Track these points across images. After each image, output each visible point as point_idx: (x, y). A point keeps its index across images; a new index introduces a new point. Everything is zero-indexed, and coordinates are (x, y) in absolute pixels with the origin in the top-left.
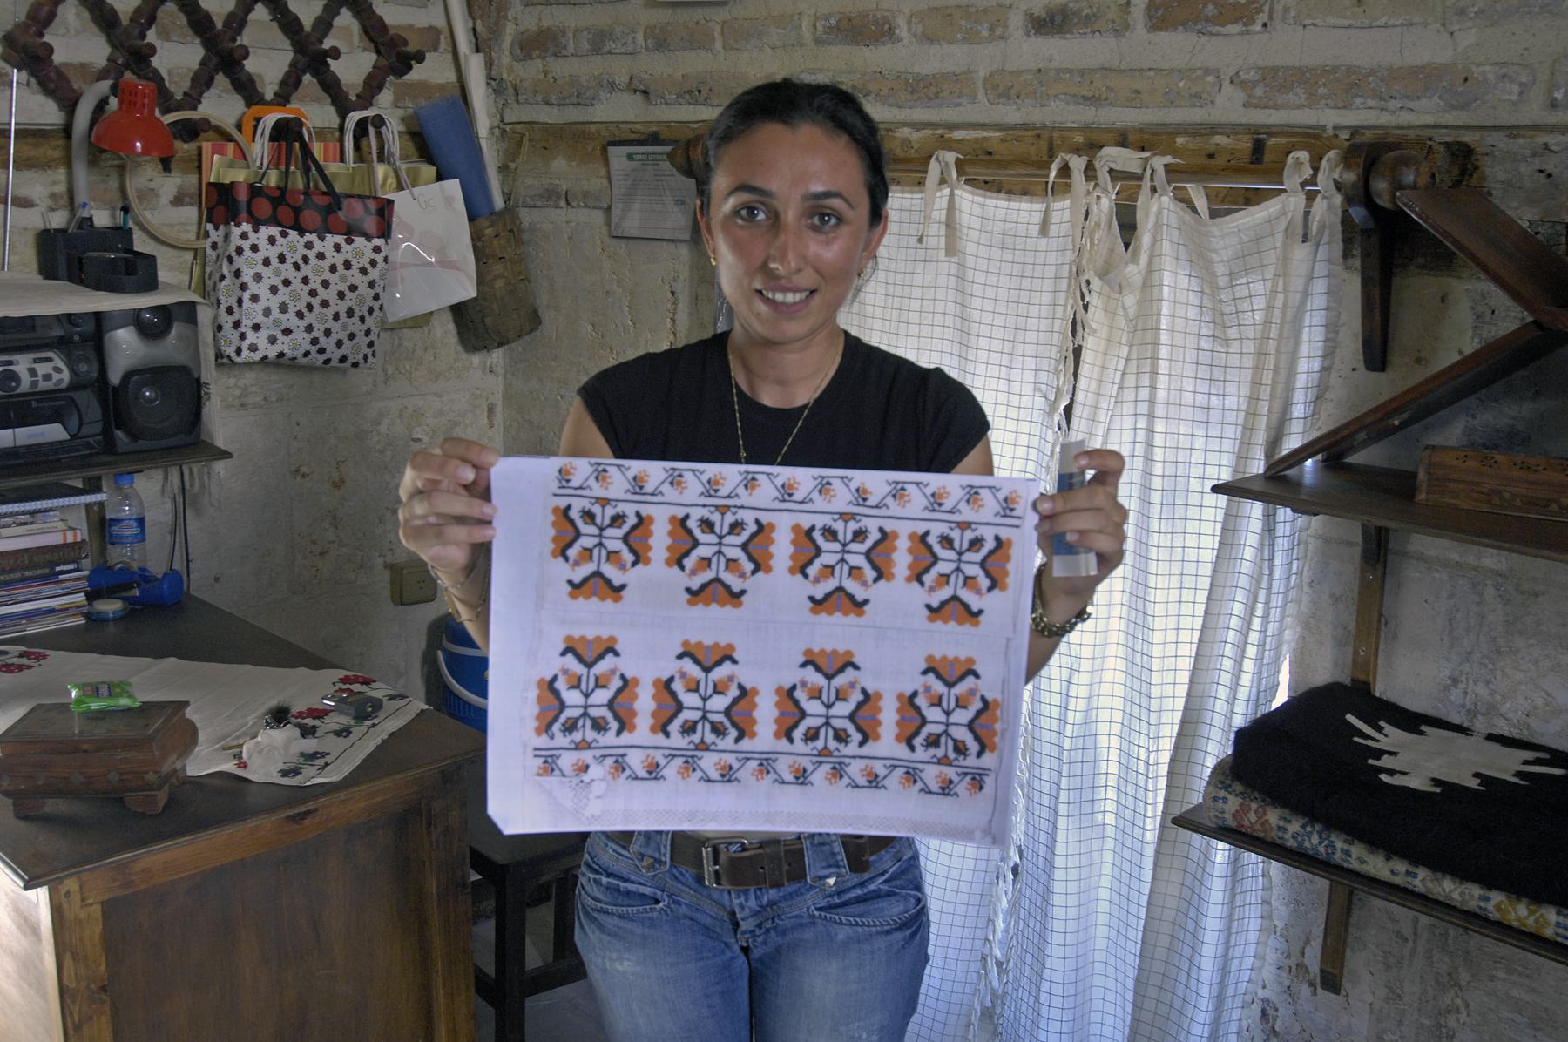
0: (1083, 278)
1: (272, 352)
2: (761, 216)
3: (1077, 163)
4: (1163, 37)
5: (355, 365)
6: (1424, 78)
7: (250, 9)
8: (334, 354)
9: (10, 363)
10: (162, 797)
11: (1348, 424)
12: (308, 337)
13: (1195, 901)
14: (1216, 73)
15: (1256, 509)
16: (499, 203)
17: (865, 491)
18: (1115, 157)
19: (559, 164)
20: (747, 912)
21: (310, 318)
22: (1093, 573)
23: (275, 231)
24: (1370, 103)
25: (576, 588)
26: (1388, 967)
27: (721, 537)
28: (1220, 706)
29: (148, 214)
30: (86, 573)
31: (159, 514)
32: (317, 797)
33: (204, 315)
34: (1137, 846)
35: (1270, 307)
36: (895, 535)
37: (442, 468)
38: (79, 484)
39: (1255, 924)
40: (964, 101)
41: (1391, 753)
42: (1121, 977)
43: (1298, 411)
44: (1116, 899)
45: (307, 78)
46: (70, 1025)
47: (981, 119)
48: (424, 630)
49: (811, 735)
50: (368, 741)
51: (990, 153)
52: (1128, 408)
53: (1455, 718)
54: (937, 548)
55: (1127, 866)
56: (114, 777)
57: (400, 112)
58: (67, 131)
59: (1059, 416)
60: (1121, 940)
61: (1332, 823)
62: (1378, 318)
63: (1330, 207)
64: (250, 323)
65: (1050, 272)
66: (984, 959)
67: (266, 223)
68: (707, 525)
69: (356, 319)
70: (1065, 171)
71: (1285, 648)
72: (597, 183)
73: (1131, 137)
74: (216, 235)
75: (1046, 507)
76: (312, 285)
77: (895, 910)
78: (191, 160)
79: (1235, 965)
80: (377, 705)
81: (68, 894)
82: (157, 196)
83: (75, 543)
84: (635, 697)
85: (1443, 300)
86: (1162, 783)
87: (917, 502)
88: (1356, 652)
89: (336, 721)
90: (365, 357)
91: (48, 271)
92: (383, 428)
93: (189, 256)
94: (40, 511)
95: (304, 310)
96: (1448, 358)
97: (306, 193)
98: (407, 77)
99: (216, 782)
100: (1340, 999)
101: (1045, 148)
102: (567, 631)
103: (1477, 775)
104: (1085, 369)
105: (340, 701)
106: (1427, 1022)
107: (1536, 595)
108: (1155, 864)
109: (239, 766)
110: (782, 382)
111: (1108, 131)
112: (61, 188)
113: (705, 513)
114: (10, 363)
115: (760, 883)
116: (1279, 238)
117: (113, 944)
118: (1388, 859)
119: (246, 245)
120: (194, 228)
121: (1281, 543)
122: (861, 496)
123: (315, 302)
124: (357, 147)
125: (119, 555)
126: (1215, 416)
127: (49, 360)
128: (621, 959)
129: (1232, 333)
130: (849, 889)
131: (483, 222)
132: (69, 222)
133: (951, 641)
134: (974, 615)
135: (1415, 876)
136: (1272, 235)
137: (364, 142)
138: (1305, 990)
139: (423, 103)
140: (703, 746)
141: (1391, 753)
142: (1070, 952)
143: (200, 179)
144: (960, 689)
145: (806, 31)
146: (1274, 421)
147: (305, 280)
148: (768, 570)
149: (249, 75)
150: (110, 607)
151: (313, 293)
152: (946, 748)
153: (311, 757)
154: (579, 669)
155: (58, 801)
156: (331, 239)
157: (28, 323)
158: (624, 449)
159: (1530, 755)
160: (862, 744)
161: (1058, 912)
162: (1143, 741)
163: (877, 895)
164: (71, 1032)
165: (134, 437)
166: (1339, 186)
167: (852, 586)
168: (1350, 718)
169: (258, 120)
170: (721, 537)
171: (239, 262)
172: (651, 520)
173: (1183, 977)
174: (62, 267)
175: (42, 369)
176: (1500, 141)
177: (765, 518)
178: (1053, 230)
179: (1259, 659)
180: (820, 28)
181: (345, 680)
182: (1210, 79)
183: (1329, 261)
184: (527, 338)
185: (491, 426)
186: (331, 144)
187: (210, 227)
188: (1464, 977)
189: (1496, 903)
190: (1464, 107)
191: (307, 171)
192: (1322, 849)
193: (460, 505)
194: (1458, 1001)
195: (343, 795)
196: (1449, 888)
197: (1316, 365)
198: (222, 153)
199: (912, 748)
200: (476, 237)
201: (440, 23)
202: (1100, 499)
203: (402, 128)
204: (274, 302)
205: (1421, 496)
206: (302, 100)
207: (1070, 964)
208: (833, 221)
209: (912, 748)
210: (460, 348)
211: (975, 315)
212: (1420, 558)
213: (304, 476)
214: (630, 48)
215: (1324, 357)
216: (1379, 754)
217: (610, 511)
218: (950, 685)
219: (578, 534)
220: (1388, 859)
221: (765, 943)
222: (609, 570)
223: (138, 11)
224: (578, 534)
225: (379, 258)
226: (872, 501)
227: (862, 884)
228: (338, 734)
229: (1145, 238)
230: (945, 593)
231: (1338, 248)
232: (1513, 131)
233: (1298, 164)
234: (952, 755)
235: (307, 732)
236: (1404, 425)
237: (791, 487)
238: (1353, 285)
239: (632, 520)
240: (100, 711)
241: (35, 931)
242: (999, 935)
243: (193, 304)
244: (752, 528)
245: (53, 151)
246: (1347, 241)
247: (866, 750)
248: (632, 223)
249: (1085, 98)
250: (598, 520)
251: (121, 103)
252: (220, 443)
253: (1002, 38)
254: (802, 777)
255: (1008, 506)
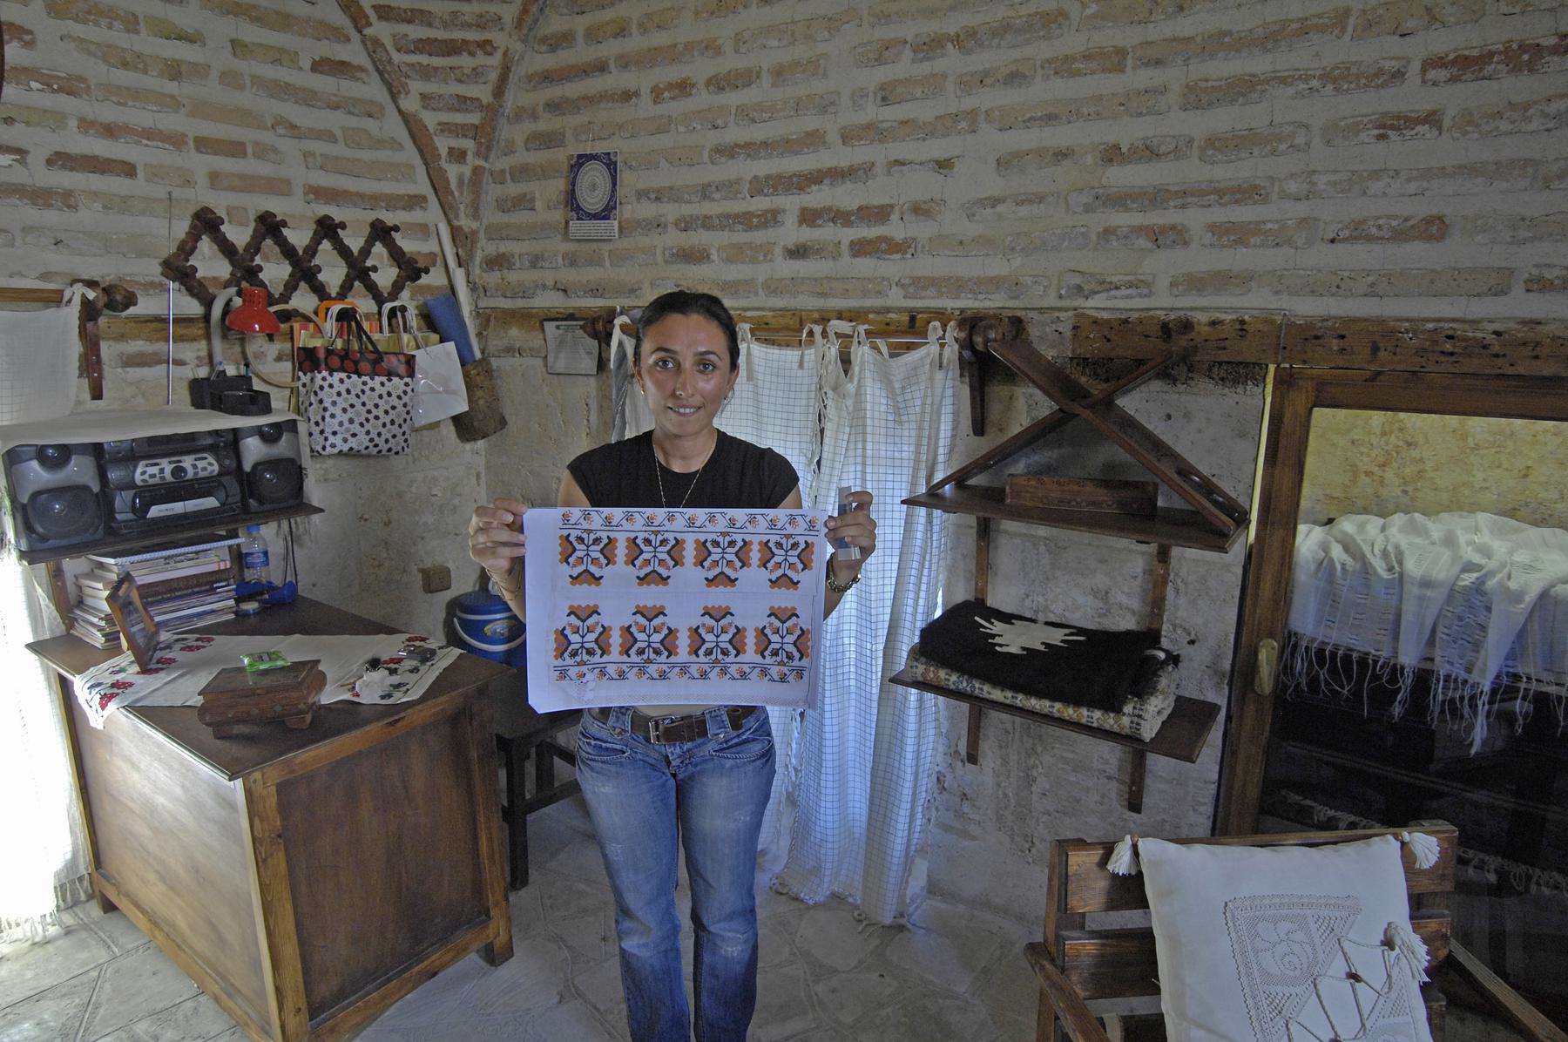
0: (823, 391)
1: (345, 448)
2: (670, 365)
3: (817, 329)
4: (859, 261)
5: (397, 453)
6: (995, 283)
7: (320, 243)
8: (384, 447)
9: (180, 461)
10: (308, 718)
11: (967, 466)
12: (368, 438)
13: (901, 723)
14: (888, 280)
15: (922, 511)
16: (478, 355)
17: (734, 520)
18: (837, 325)
19: (514, 332)
20: (675, 756)
21: (368, 426)
22: (858, 557)
23: (343, 375)
24: (969, 296)
25: (574, 579)
26: (1001, 747)
27: (655, 548)
28: (909, 617)
29: (260, 367)
30: (234, 587)
31: (277, 548)
32: (405, 710)
33: (302, 427)
34: (868, 696)
35: (924, 404)
36: (751, 543)
37: (494, 515)
38: (224, 533)
39: (932, 732)
40: (751, 295)
41: (999, 636)
42: (863, 767)
43: (941, 458)
44: (858, 725)
45: (357, 283)
46: (259, 859)
47: (762, 305)
48: (444, 606)
49: (709, 653)
50: (430, 674)
51: (767, 324)
52: (851, 460)
53: (1028, 615)
54: (774, 549)
55: (863, 707)
56: (278, 708)
57: (415, 303)
58: (207, 318)
59: (814, 466)
60: (863, 748)
61: (973, 674)
62: (979, 410)
63: (952, 351)
64: (331, 431)
65: (805, 388)
66: (787, 766)
67: (337, 370)
68: (648, 542)
69: (396, 426)
70: (811, 333)
71: (940, 584)
72: (537, 343)
73: (844, 315)
74: (305, 379)
75: (832, 524)
76: (368, 407)
77: (757, 748)
78: (286, 334)
79: (923, 755)
80: (433, 652)
81: (255, 781)
82: (265, 356)
83: (226, 569)
84: (610, 637)
85: (1011, 398)
86: (880, 661)
87: (762, 524)
88: (977, 584)
89: (409, 664)
90: (403, 448)
91: (198, 403)
92: (414, 490)
93: (288, 392)
94: (203, 551)
95: (364, 422)
96: (1015, 429)
97: (360, 352)
98: (418, 282)
99: (339, 706)
100: (978, 766)
101: (798, 320)
102: (570, 603)
103: (1043, 643)
104: (826, 440)
105: (410, 652)
106: (1022, 774)
107: (1065, 548)
108: (879, 705)
109: (353, 695)
110: (684, 458)
111: (832, 311)
112: (204, 353)
113: (646, 535)
114: (180, 461)
115: (682, 739)
116: (927, 367)
117: (284, 809)
118: (1002, 691)
119: (326, 384)
120: (291, 375)
121: (936, 529)
122: (732, 522)
123: (371, 417)
124: (390, 324)
125: (251, 575)
126: (897, 463)
127: (205, 458)
128: (604, 786)
129: (904, 418)
130: (732, 739)
131: (469, 367)
132: (210, 374)
133: (783, 598)
134: (795, 584)
135: (1016, 698)
136: (923, 366)
137: (394, 321)
138: (959, 764)
139: (429, 297)
140: (649, 661)
141: (999, 636)
142: (836, 757)
143: (293, 345)
144: (789, 624)
145: (659, 257)
146: (930, 465)
147: (364, 404)
148: (683, 564)
149: (321, 282)
150: (251, 606)
151: (369, 412)
152: (782, 656)
153: (397, 686)
154: (578, 623)
155: (241, 726)
156: (378, 379)
157: (192, 437)
158: (596, 502)
159: (1067, 631)
160: (736, 656)
161: (828, 736)
162: (868, 639)
163: (747, 741)
164: (260, 864)
165: (261, 503)
166: (956, 340)
167: (728, 571)
168: (977, 618)
169: (328, 309)
170: (655, 548)
171: (321, 394)
172: (616, 540)
173: (896, 764)
174: (207, 400)
175: (200, 464)
176: (1035, 315)
177: (679, 537)
178: (806, 365)
179: (927, 591)
180: (667, 255)
181: (410, 640)
182: (885, 283)
183: (953, 379)
184: (498, 433)
185: (479, 485)
186: (374, 323)
187: (301, 374)
188: (1039, 749)
189: (1057, 708)
190: (1016, 298)
191: (360, 339)
192: (968, 689)
193: (505, 536)
194: (1037, 762)
195: (419, 707)
196: (1034, 703)
197: (949, 434)
198: (306, 329)
199: (764, 657)
200: (466, 375)
201: (437, 249)
202: (861, 518)
203: (416, 312)
204: (345, 418)
205: (1008, 501)
206: (353, 297)
207: (836, 763)
208: (711, 368)
209: (764, 657)
210: (458, 440)
211: (765, 413)
212: (1006, 532)
213: (366, 520)
214: (554, 265)
215: (953, 430)
216: (993, 636)
217: (592, 537)
218: (783, 622)
219: (575, 550)
220: (1002, 691)
221: (685, 771)
222: (592, 569)
223: (249, 245)
224: (575, 550)
225: (408, 389)
226: (738, 525)
227: (738, 736)
228: (411, 671)
229: (856, 369)
230: (779, 573)
231: (958, 372)
232: (1041, 310)
233: (935, 328)
234: (785, 660)
235: (393, 672)
236: (995, 464)
237: (693, 519)
238: (966, 391)
239: (605, 541)
240: (266, 670)
241: (232, 807)
242: (794, 751)
243: (295, 421)
244: (673, 542)
245: (198, 330)
246: (962, 368)
247: (739, 659)
248: (560, 364)
249: (819, 294)
250: (586, 542)
251: (244, 301)
252: (315, 503)
253: (771, 260)
254: (704, 675)
255: (811, 525)
